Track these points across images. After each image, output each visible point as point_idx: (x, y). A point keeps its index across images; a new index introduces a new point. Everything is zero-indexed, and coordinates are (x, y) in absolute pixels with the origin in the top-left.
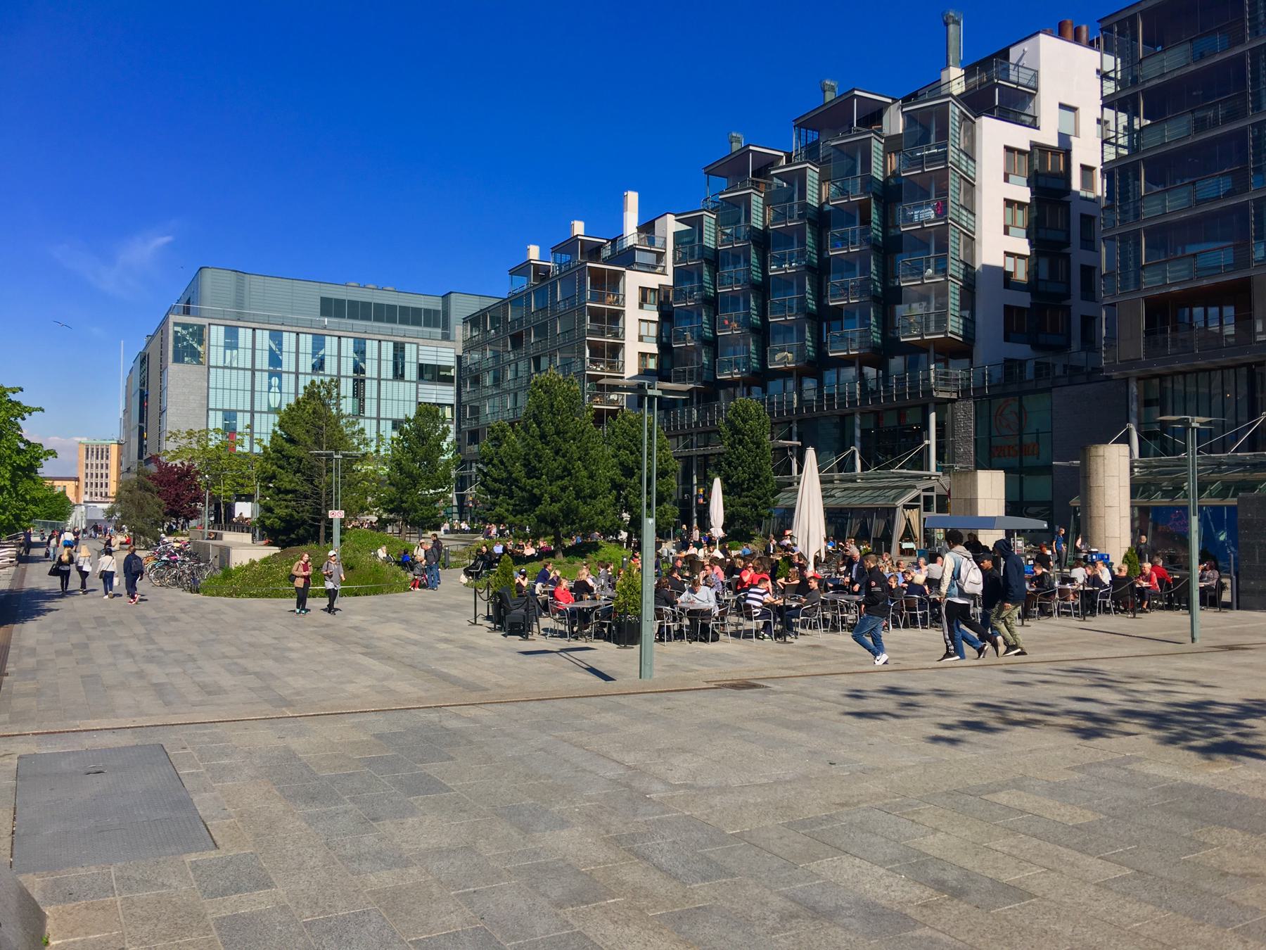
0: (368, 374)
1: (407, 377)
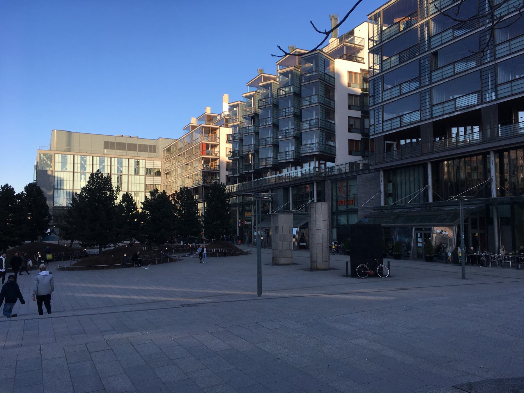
0: (124, 173)
1: (141, 174)
